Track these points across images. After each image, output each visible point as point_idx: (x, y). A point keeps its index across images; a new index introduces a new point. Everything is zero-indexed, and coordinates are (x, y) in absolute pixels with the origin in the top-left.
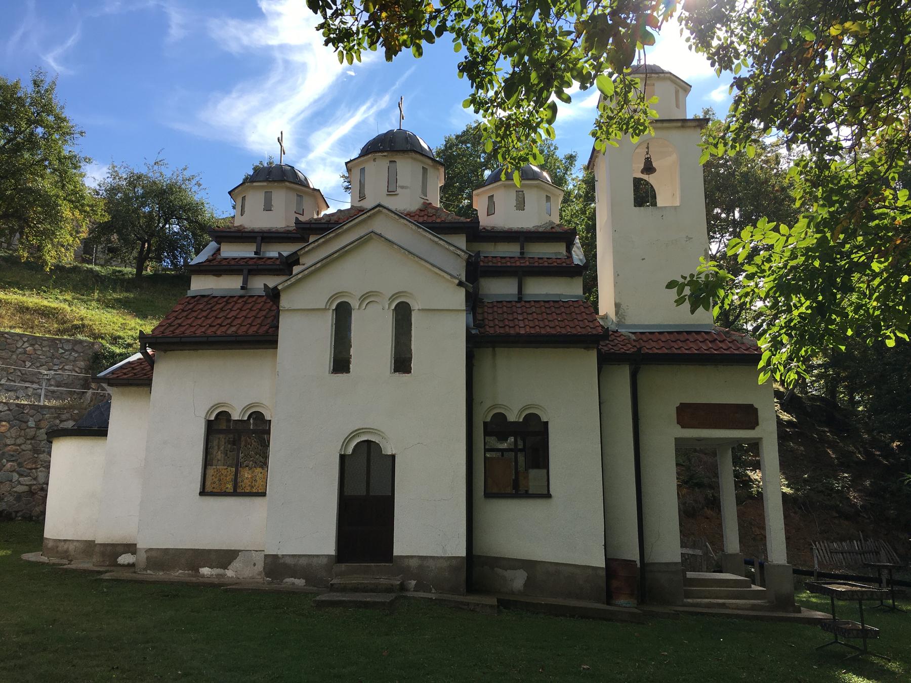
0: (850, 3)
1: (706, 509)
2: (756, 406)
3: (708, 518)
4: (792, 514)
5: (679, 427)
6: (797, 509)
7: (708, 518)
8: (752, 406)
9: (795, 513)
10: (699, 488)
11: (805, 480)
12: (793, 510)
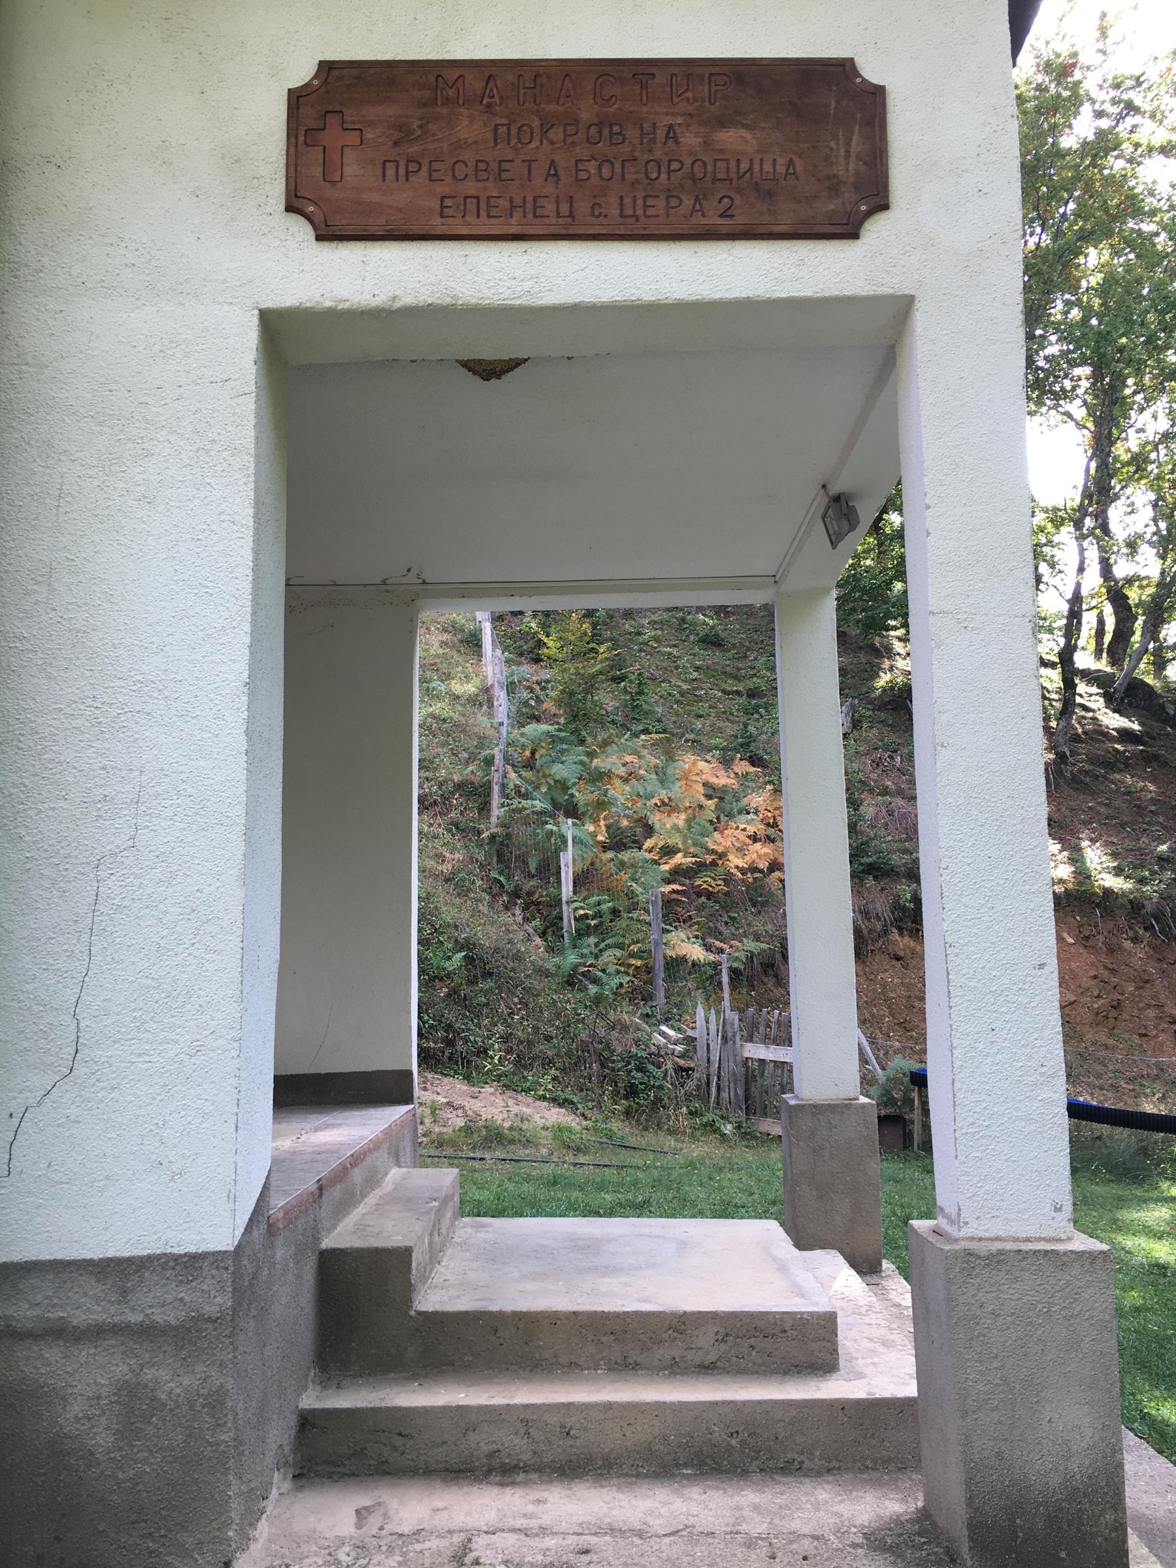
0: (1170, 655)
1: (895, 935)
2: (871, 71)
3: (898, 958)
4: (1128, 944)
5: (301, 229)
6: (1141, 932)
7: (898, 958)
8: (844, 69)
9: (1135, 940)
10: (876, 878)
11: (1162, 860)
12: (1131, 934)
